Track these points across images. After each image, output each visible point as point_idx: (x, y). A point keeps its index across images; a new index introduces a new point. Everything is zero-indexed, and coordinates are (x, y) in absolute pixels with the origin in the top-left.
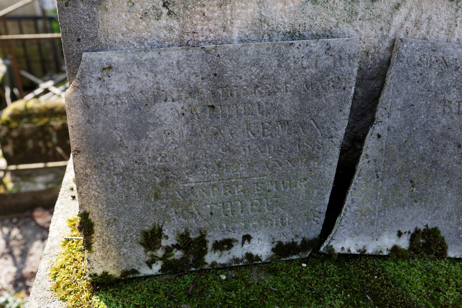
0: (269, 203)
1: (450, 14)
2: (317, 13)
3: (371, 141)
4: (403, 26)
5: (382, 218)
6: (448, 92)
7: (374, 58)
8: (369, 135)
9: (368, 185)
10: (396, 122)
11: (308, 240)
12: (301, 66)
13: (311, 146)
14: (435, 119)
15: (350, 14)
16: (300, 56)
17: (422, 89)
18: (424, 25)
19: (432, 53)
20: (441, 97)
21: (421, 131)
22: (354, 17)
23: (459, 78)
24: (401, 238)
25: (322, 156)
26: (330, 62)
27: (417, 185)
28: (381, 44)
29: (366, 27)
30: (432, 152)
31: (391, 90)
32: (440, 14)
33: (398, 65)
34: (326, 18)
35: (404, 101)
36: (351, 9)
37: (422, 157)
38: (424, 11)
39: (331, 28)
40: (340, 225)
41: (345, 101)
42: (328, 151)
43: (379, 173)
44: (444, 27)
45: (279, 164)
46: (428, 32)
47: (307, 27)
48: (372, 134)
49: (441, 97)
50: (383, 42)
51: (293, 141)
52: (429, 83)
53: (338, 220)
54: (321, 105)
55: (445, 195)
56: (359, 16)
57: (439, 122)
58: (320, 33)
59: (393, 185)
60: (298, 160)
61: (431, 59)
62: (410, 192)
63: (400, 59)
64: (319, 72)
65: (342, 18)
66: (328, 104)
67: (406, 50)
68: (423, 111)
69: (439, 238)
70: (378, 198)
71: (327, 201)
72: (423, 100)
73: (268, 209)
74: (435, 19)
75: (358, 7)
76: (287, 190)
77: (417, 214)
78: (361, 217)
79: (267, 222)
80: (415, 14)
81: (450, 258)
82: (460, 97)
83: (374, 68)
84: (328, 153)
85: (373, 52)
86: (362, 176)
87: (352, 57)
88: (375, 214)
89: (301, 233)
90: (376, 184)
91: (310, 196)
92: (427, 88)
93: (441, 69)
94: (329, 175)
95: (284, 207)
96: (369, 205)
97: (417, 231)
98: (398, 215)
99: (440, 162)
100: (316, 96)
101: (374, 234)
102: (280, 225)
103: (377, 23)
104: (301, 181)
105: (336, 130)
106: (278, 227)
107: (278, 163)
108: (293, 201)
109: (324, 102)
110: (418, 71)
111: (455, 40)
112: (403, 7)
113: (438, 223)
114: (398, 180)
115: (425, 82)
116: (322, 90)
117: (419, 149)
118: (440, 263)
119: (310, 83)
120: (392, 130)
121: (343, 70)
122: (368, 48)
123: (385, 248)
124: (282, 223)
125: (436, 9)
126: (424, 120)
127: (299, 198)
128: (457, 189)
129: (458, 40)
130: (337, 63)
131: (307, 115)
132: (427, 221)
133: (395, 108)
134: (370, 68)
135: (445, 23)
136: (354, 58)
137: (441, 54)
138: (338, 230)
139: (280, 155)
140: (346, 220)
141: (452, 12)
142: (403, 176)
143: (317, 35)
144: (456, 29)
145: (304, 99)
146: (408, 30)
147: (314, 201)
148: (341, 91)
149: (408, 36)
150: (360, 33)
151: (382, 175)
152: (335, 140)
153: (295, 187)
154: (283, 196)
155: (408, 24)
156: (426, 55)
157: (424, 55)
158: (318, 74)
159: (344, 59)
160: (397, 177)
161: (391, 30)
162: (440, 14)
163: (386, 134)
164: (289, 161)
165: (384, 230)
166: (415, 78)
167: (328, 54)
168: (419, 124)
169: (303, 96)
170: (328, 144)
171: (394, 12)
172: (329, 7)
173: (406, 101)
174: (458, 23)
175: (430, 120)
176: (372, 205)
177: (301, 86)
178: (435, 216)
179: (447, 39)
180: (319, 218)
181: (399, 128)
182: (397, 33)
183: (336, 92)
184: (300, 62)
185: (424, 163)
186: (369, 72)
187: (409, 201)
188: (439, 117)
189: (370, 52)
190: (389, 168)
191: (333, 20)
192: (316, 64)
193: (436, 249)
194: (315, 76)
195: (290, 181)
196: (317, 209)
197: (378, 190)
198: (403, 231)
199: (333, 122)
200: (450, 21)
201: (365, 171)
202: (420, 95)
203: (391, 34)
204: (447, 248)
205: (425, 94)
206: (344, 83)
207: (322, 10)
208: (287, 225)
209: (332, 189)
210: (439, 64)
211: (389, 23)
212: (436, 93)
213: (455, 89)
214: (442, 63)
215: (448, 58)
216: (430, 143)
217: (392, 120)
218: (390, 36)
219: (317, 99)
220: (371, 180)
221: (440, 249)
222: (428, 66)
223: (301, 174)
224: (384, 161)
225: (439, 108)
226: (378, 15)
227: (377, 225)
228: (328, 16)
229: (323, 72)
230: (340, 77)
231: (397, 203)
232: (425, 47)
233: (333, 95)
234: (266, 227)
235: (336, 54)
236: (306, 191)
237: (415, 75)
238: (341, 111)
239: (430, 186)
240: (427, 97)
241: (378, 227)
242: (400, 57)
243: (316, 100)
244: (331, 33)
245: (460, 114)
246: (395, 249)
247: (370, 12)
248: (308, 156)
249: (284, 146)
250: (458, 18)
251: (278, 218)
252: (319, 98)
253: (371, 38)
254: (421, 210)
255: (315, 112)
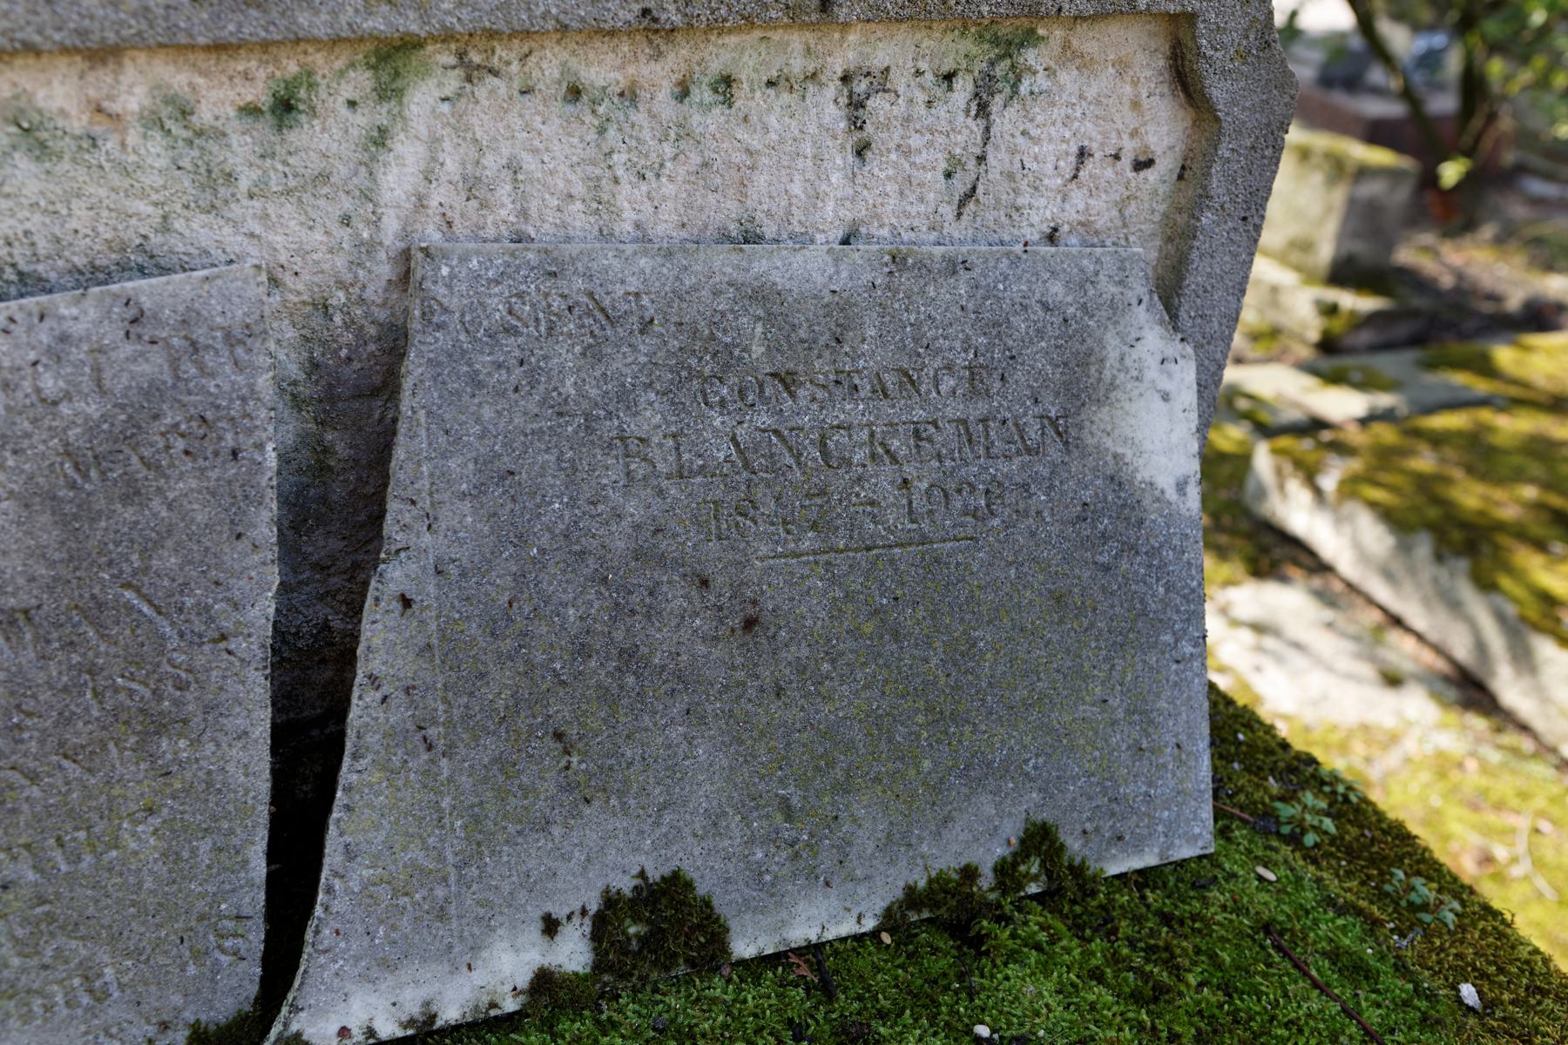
0: (19, 932)
1: (581, 146)
2: (65, 191)
3: (379, 626)
4: (425, 202)
5: (475, 887)
6: (628, 408)
7: (353, 322)
8: (369, 602)
9: (400, 783)
10: (461, 542)
11: (212, 1028)
12: (34, 398)
13: (147, 685)
14: (601, 508)
15: (203, 179)
16: (23, 359)
17: (536, 411)
18: (503, 191)
19: (548, 284)
20: (608, 428)
21: (559, 556)
22: (222, 191)
23: (659, 354)
24: (558, 938)
25: (199, 713)
26: (154, 366)
27: (580, 745)
28: (361, 273)
29: (282, 220)
30: (614, 619)
31: (423, 433)
32: (547, 150)
33: (430, 339)
34: (112, 206)
35: (476, 463)
36: (200, 163)
37: (582, 645)
38: (485, 143)
39: (145, 237)
40: (316, 951)
41: (246, 497)
42: (221, 688)
43: (432, 732)
44: (574, 191)
45: (26, 776)
46: (524, 214)
47: (43, 247)
48: (377, 599)
49: (608, 428)
50: (368, 264)
51: (65, 679)
52: (555, 389)
53: (309, 936)
54: (152, 529)
55: (686, 758)
56: (244, 184)
57: (619, 516)
58: (105, 262)
59: (495, 761)
60: (104, 747)
61: (549, 306)
62: (560, 772)
63: (435, 319)
64: (117, 410)
65: (174, 198)
66: (183, 519)
67: (449, 287)
68: (552, 486)
69: (690, 905)
70: (446, 820)
71: (259, 867)
72: (547, 450)
73: (19, 954)
74: (533, 167)
75: (229, 154)
76: (84, 865)
77: (601, 843)
78: (394, 902)
79: (27, 1004)
80: (457, 158)
81: (742, 963)
82: (674, 418)
83: (365, 356)
84: (224, 696)
85: (343, 300)
86: (370, 757)
87: (240, 336)
88: (445, 879)
89: (178, 1011)
90: (427, 773)
91: (182, 870)
92: (553, 407)
93: (592, 332)
94: (247, 775)
95: (83, 930)
96: (416, 853)
97: (611, 901)
98: (532, 863)
99: (647, 650)
100: (126, 499)
101: (456, 950)
102: (86, 1000)
103: (322, 202)
104: (136, 822)
105: (236, 606)
106: (80, 1012)
107: (22, 772)
108: (119, 901)
109: (164, 514)
110: (510, 352)
111: (628, 227)
112: (402, 136)
113: (681, 855)
114: (507, 741)
115: (542, 388)
116: (145, 472)
117: (565, 619)
118: (709, 988)
119: (90, 453)
120: (453, 570)
121: (212, 390)
122: (316, 289)
123: (508, 988)
124: (91, 991)
125: (525, 134)
126: (561, 517)
127: (140, 884)
128: (724, 726)
129: (638, 226)
130: (183, 368)
131: (101, 574)
132: (642, 859)
133: (449, 493)
134: (349, 359)
135: (573, 177)
136: (249, 341)
137: (579, 283)
138: (311, 970)
139: (22, 741)
140: (338, 926)
141: (588, 138)
142: (522, 722)
143: (95, 269)
144: (620, 193)
145: (76, 517)
146: (449, 214)
147: (205, 880)
148: (224, 463)
149: (453, 233)
150: (269, 243)
151: (447, 734)
152: (239, 644)
153: (117, 847)
154: (71, 891)
155: (439, 195)
156: (529, 294)
157: (520, 295)
158: (114, 416)
159: (208, 347)
160: (503, 729)
161: (385, 219)
162: (547, 150)
163: (431, 589)
164: (66, 756)
165: (488, 926)
166: (504, 377)
167: (139, 337)
168: (547, 535)
169: (69, 509)
170: (214, 665)
171: (373, 158)
172: (107, 166)
173: (485, 463)
174: (620, 172)
175: (584, 513)
176: (427, 849)
177: (52, 472)
178: (665, 835)
179: (597, 228)
180: (242, 936)
181: (476, 559)
182: (409, 229)
183: (203, 470)
184: (26, 384)
185: (593, 664)
186: (347, 372)
187: (561, 805)
188: (615, 497)
189: (330, 301)
190: (467, 707)
191: (143, 207)
192: (99, 382)
193: (686, 944)
194: (105, 426)
195: (88, 828)
196: (223, 906)
197: (441, 792)
198: (559, 912)
199: (217, 583)
200: (590, 169)
201: (377, 737)
202: (533, 433)
203: (390, 233)
204: (728, 930)
205: (550, 428)
206: (229, 436)
207: (81, 179)
208: (116, 995)
209: (271, 822)
210: (580, 318)
211: (366, 197)
212: (588, 416)
213: (652, 396)
214: (589, 313)
215: (608, 293)
216: (599, 592)
217: (446, 536)
218: (387, 243)
219: (131, 510)
220: (406, 761)
221: (702, 940)
222: (542, 329)
223: (129, 794)
224: (445, 685)
225: (607, 469)
226: (316, 173)
227: (460, 917)
228: (113, 195)
229: (132, 406)
230: (209, 415)
231: (520, 822)
232: (519, 267)
233: (194, 484)
234: (25, 1023)
235: (173, 333)
236: (163, 855)
237: (499, 366)
238: (239, 536)
239: (628, 737)
240: (559, 435)
241: (464, 921)
242: (432, 314)
243: (129, 514)
244: (152, 257)
245: (686, 474)
246: (544, 981)
247: (280, 167)
248: (142, 723)
249: (29, 705)
250: (615, 157)
251: (70, 977)
252: (141, 504)
253: (315, 257)
254: (610, 827)
255: (135, 557)
